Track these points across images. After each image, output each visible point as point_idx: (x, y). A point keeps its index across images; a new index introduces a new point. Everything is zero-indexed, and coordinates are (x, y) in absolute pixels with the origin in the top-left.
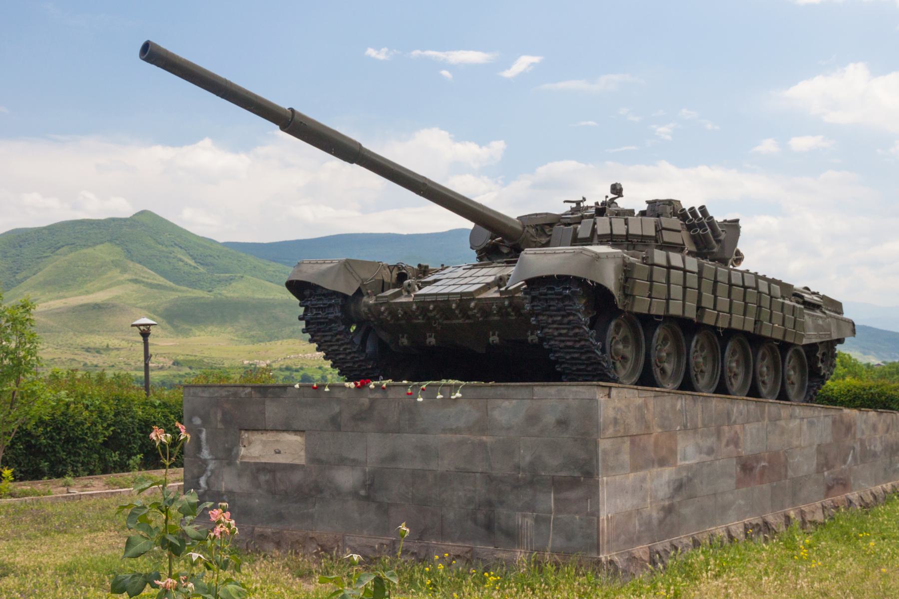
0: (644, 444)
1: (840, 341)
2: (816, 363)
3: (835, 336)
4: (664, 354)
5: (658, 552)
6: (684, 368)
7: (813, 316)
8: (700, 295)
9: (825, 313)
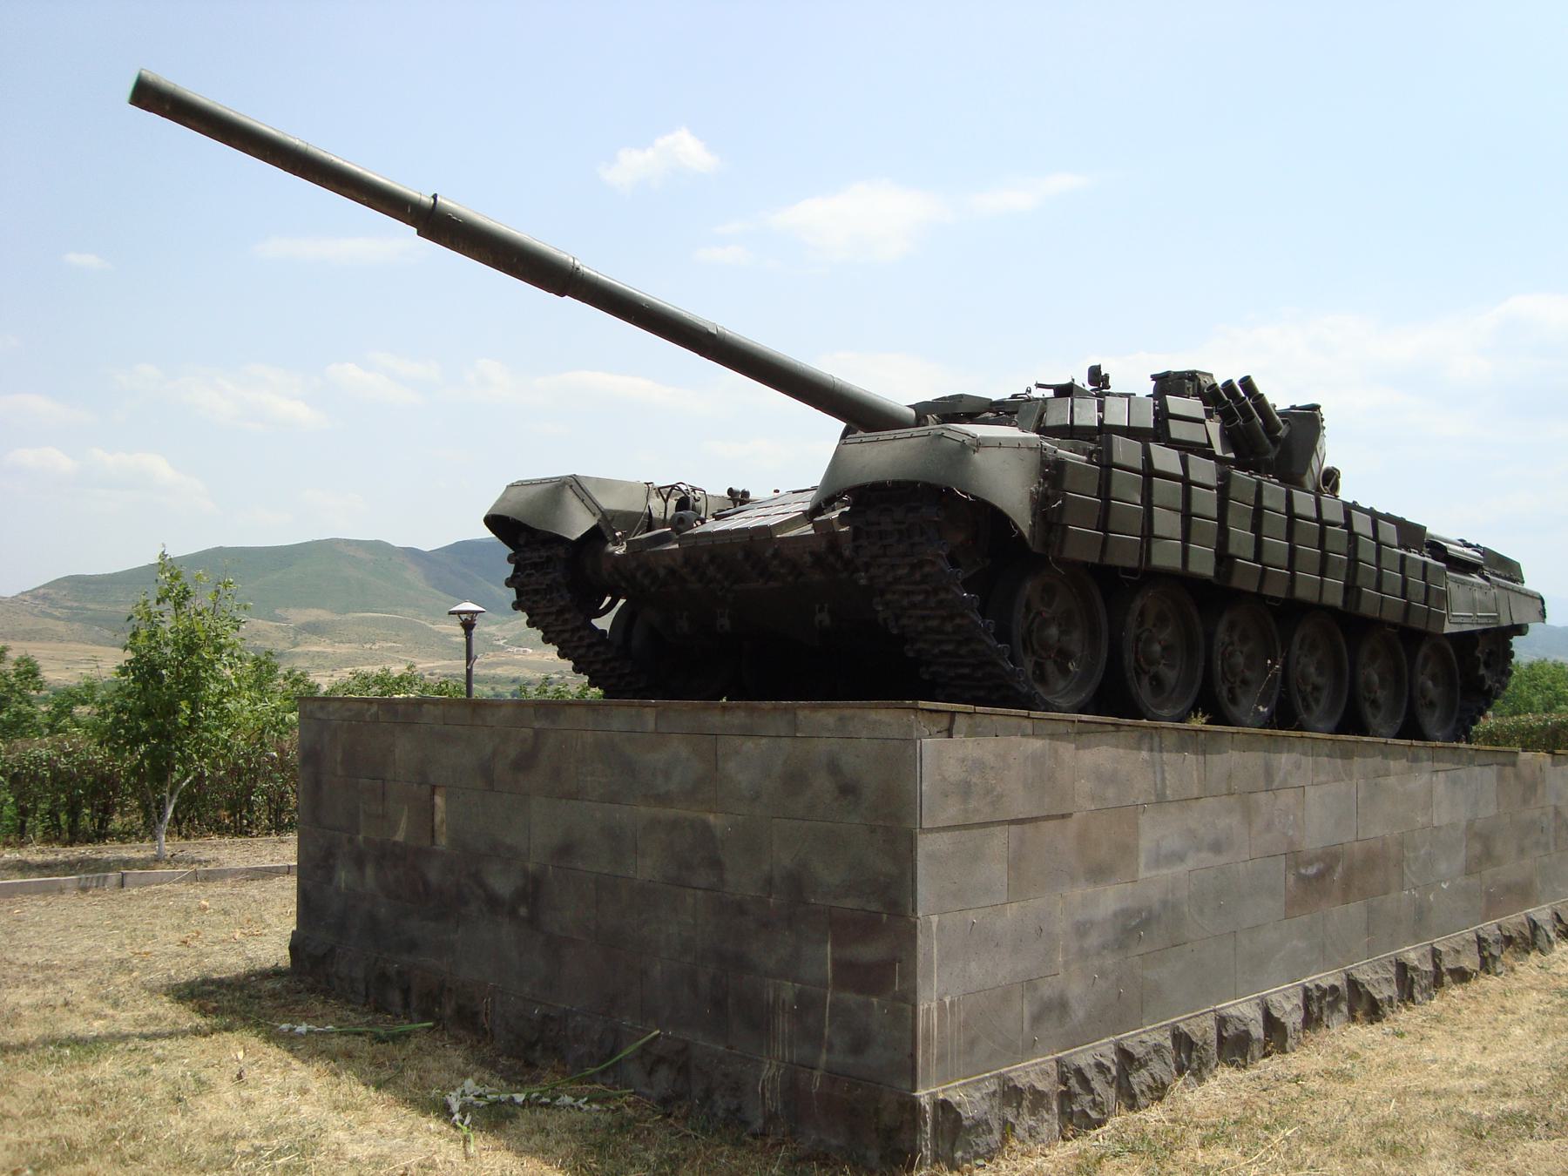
0: (1026, 844)
1: (1520, 630)
2: (1477, 667)
3: (1505, 622)
4: (1157, 648)
5: (1079, 1072)
6: (1200, 673)
7: (1464, 583)
8: (1223, 531)
9: (1487, 579)
